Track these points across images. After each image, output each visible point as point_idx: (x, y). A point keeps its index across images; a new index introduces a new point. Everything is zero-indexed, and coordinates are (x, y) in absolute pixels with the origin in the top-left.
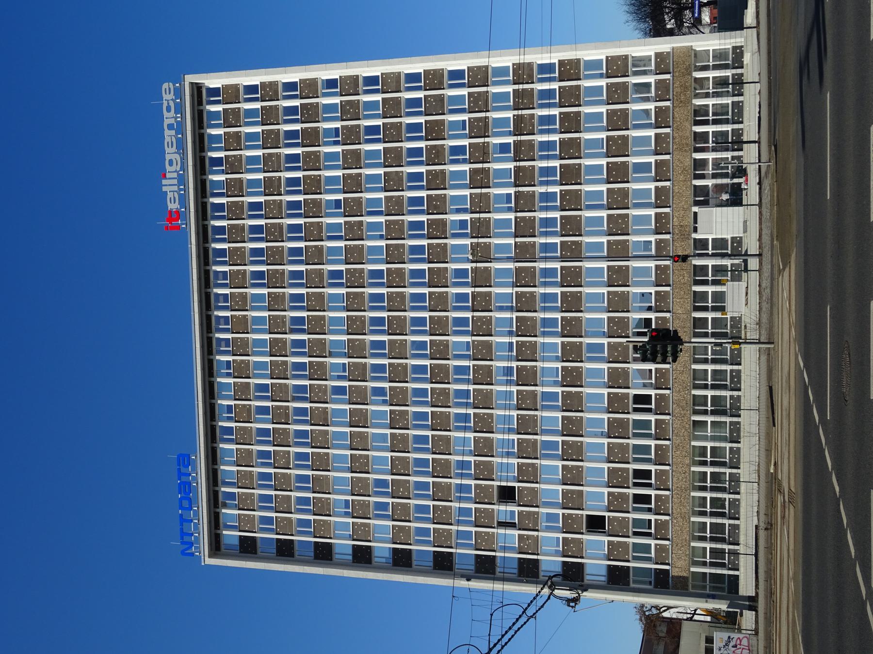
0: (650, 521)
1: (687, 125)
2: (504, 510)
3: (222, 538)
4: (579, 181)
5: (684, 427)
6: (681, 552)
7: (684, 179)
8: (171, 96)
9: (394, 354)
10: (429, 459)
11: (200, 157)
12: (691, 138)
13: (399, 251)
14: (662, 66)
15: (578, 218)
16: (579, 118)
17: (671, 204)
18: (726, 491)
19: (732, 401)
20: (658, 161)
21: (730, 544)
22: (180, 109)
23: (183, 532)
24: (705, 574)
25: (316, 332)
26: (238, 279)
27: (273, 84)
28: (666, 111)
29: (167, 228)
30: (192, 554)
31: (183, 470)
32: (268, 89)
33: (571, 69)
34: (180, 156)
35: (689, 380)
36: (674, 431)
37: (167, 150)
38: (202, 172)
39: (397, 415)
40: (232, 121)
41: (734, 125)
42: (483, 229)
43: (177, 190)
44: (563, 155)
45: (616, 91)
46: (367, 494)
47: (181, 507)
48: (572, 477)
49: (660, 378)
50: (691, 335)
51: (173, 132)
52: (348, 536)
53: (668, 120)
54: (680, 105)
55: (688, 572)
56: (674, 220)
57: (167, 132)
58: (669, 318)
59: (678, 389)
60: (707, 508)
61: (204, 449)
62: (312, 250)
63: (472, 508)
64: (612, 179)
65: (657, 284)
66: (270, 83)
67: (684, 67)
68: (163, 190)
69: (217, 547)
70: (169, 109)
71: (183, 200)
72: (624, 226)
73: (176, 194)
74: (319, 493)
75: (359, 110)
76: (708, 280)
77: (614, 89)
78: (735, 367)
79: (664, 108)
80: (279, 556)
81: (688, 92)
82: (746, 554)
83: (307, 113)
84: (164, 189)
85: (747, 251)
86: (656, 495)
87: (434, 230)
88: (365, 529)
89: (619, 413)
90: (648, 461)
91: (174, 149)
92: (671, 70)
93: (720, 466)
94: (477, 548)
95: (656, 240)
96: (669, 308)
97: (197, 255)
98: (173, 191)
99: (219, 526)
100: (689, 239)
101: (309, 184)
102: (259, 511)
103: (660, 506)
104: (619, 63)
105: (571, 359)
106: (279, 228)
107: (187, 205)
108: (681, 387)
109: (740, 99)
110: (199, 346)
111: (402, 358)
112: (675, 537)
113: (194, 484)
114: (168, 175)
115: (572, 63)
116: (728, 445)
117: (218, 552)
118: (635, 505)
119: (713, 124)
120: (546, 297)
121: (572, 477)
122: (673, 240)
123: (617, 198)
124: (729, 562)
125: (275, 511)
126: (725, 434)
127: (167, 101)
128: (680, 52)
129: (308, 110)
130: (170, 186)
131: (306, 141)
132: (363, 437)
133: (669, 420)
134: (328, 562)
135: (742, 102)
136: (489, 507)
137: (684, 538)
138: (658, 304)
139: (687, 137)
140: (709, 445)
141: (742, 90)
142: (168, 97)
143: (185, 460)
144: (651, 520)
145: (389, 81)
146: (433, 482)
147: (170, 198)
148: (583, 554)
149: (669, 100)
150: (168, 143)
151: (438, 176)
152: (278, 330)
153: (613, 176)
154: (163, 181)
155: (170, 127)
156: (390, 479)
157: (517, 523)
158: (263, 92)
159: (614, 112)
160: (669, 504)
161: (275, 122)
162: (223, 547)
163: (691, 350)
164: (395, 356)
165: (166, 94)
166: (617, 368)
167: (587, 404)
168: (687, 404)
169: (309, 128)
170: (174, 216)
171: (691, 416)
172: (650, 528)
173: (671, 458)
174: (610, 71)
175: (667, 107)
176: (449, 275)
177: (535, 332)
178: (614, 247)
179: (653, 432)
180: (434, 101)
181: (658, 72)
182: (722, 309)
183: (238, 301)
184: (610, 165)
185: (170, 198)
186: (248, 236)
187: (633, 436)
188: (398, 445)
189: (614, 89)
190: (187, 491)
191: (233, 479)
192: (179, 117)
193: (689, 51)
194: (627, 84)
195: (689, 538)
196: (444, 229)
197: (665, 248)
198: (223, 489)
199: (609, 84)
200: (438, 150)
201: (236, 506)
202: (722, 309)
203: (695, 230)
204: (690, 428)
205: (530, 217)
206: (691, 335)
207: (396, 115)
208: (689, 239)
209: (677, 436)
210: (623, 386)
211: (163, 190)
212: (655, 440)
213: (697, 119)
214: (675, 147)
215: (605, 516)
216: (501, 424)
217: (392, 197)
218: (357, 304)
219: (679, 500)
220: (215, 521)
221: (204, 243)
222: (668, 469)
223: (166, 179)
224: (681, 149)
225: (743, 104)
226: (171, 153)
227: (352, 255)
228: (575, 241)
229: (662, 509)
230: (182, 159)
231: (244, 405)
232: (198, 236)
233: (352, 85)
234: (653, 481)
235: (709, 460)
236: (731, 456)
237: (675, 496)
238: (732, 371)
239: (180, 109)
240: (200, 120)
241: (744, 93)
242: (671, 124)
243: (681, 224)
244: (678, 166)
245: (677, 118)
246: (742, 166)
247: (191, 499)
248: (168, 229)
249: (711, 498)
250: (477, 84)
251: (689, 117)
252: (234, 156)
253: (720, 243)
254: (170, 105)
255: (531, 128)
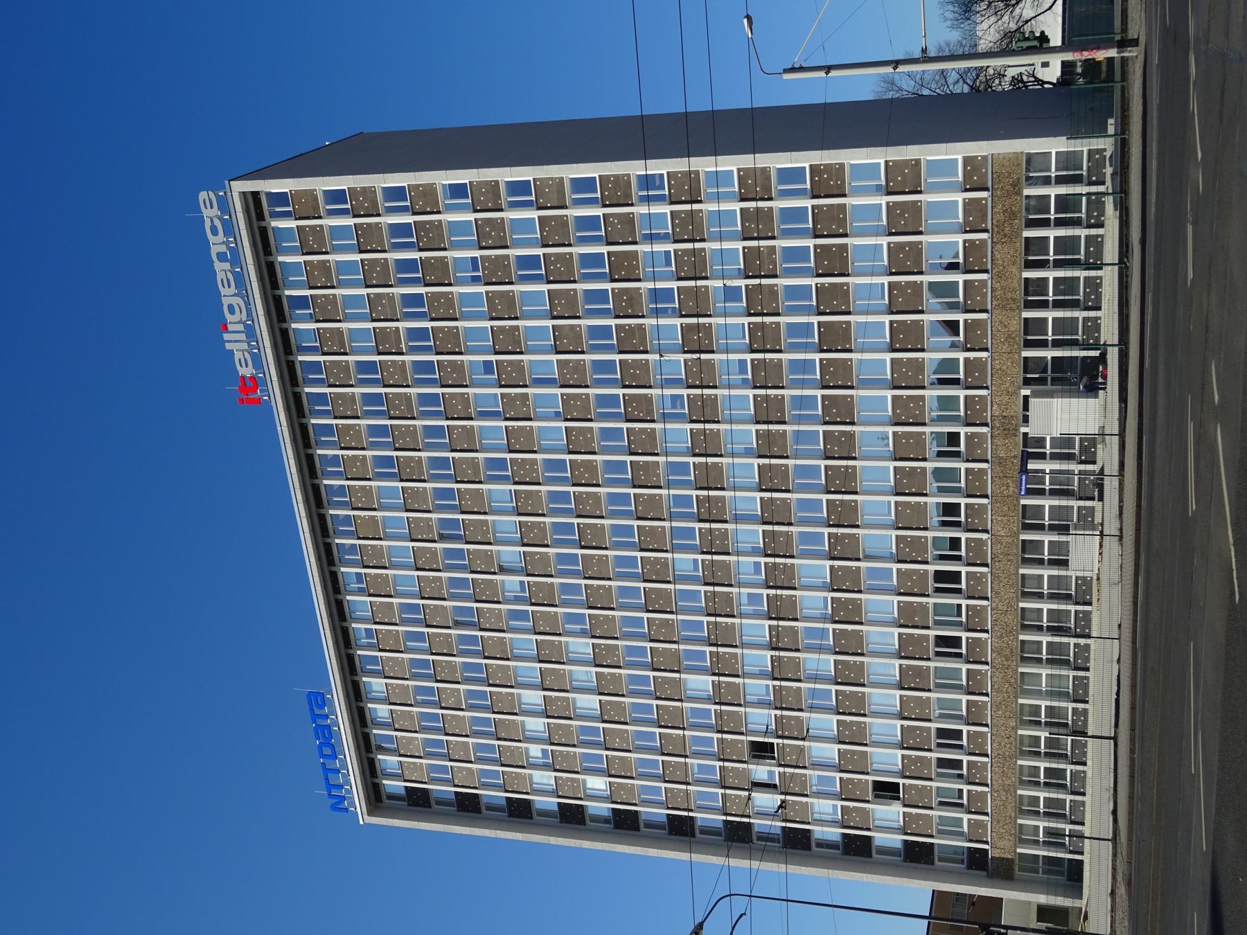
0: (959, 606)
1: (1013, 270)
2: (761, 771)
3: (345, 604)
4: (848, 346)
5: (1008, 681)
6: (1004, 831)
7: (1009, 350)
8: (215, 212)
9: (592, 573)
10: (608, 290)
11: (274, 296)
12: (1020, 290)
13: (585, 437)
14: (975, 178)
15: (849, 399)
16: (845, 254)
17: (989, 383)
18: (1073, 495)
19: (1090, 164)
20: (969, 321)
21: (1073, 823)
22: (229, 229)
23: (245, 385)
24: (1037, 856)
25: (478, 541)
26: (356, 467)
27: (368, 190)
28: (981, 248)
29: (242, 401)
30: (346, 810)
31: (317, 712)
32: (361, 199)
33: (829, 179)
34: (244, 300)
35: (1015, 623)
36: (994, 685)
37: (224, 291)
38: (281, 318)
39: (604, 649)
40: (313, 244)
41: (1091, 187)
42: (708, 411)
43: (247, 348)
44: (822, 308)
45: (902, 215)
46: (571, 743)
47: (323, 756)
48: (850, 736)
49: (974, 617)
50: (1021, 266)
51: (227, 266)
52: (512, 509)
53: (985, 260)
54: (1003, 240)
55: (1013, 854)
56: (994, 408)
57: (219, 266)
58: (987, 540)
59: (999, 634)
60: (1040, 748)
61: (320, 580)
62: (458, 431)
63: (673, 288)
64: (898, 345)
65: (968, 562)
66: (364, 189)
67: (1008, 181)
68: (227, 348)
69: (376, 798)
70: (214, 231)
71: (257, 361)
72: (917, 412)
73: (228, 273)
74: (505, 740)
75: (505, 233)
76: (1047, 339)
77: (898, 212)
78: (1092, 314)
79: (977, 242)
80: (461, 811)
81: (1016, 221)
82: (1112, 435)
83: (426, 235)
84: (228, 346)
85: (1105, 342)
86: (965, 282)
87: (634, 409)
88: (573, 785)
89: (915, 658)
90: (957, 491)
91: (233, 290)
92: (990, 184)
93: (1072, 307)
94: (701, 518)
95: (964, 199)
96: (987, 526)
97: (286, 407)
98: (243, 351)
99: (323, 504)
100: (1016, 436)
101: (442, 340)
102: (359, 387)
103: (975, 774)
104: (906, 171)
105: (844, 588)
106: (406, 400)
107: (259, 337)
108: (1003, 631)
109: (1100, 231)
110: (314, 561)
111: (603, 579)
112: (996, 813)
113: (265, 398)
114: (230, 327)
115: (832, 170)
116: (1071, 706)
117: (380, 804)
118: (939, 770)
119: (1055, 266)
120: (791, 253)
121: (850, 736)
122: (992, 437)
123: (907, 372)
124: (1070, 844)
125: (382, 385)
126: (1067, 658)
127: (209, 219)
128: (1004, 158)
129: (427, 231)
130: (235, 342)
131: (430, 278)
132: (509, 298)
133: (986, 671)
134: (528, 821)
135: (1102, 236)
136: (721, 527)
137: (1008, 814)
138: (970, 520)
139: (1014, 290)
140: (1044, 704)
141: (1103, 218)
142: (210, 213)
143: (318, 700)
144: (961, 605)
145: (547, 190)
146: (620, 361)
147: (240, 360)
148: (870, 825)
149: (986, 231)
150: (222, 280)
151: (634, 333)
152: (422, 536)
153: (900, 341)
154: (224, 335)
155: (222, 257)
156: (546, 290)
157: (778, 784)
158: (354, 203)
159: (900, 246)
160: (987, 772)
161: (379, 248)
162: (384, 798)
163: (1017, 584)
164: (593, 575)
165: (206, 208)
166: (912, 603)
167: (854, 224)
168: (1012, 652)
169: (432, 258)
170: (249, 384)
171: (1018, 634)
172: (959, 615)
173: (989, 717)
174: (891, 184)
175: (983, 242)
176: (661, 471)
177: (791, 551)
178: (904, 441)
179: (962, 413)
180: (619, 223)
181: (968, 187)
182: (1064, 563)
183: (361, 497)
184: (895, 325)
185: (240, 360)
186: (361, 408)
187: (936, 687)
188: (574, 411)
189: (898, 212)
190: (320, 703)
191: (299, 276)
192: (232, 242)
193: (1017, 157)
194: (919, 204)
195: (1016, 814)
196: (649, 408)
197: (980, 445)
198: (300, 358)
199: (891, 204)
200: (631, 295)
201: (311, 317)
202: (1064, 563)
203: (1026, 420)
204: (1016, 682)
205: (776, 396)
206: (1021, 266)
207: (561, 242)
208: (1016, 436)
209: (997, 692)
210: (920, 625)
211: (227, 348)
212: (964, 313)
213: (1030, 258)
214: (994, 303)
215: (899, 783)
216: (718, 265)
217: (568, 361)
218: (531, 505)
219: (1002, 770)
220: (370, 770)
221: (299, 417)
222: (986, 278)
223: (229, 332)
224: (1004, 307)
225: (1102, 239)
226: (228, 296)
227: (518, 440)
228: (845, 431)
229: (978, 778)
230: (247, 304)
231: (389, 630)
232: (263, 284)
233: (490, 196)
234: (963, 553)
235: (1047, 523)
236: (1075, 718)
237: (995, 765)
238: (1086, 320)
239: (229, 229)
240: (263, 242)
241: (1106, 223)
242: (989, 267)
243: (1004, 414)
244: (999, 331)
245: (998, 260)
246: (1114, 38)
247: (333, 746)
248: (243, 403)
249: (1048, 610)
250: (683, 198)
251: (1018, 259)
252: (324, 296)
253: (1066, 441)
254: (215, 224)
255: (771, 267)
